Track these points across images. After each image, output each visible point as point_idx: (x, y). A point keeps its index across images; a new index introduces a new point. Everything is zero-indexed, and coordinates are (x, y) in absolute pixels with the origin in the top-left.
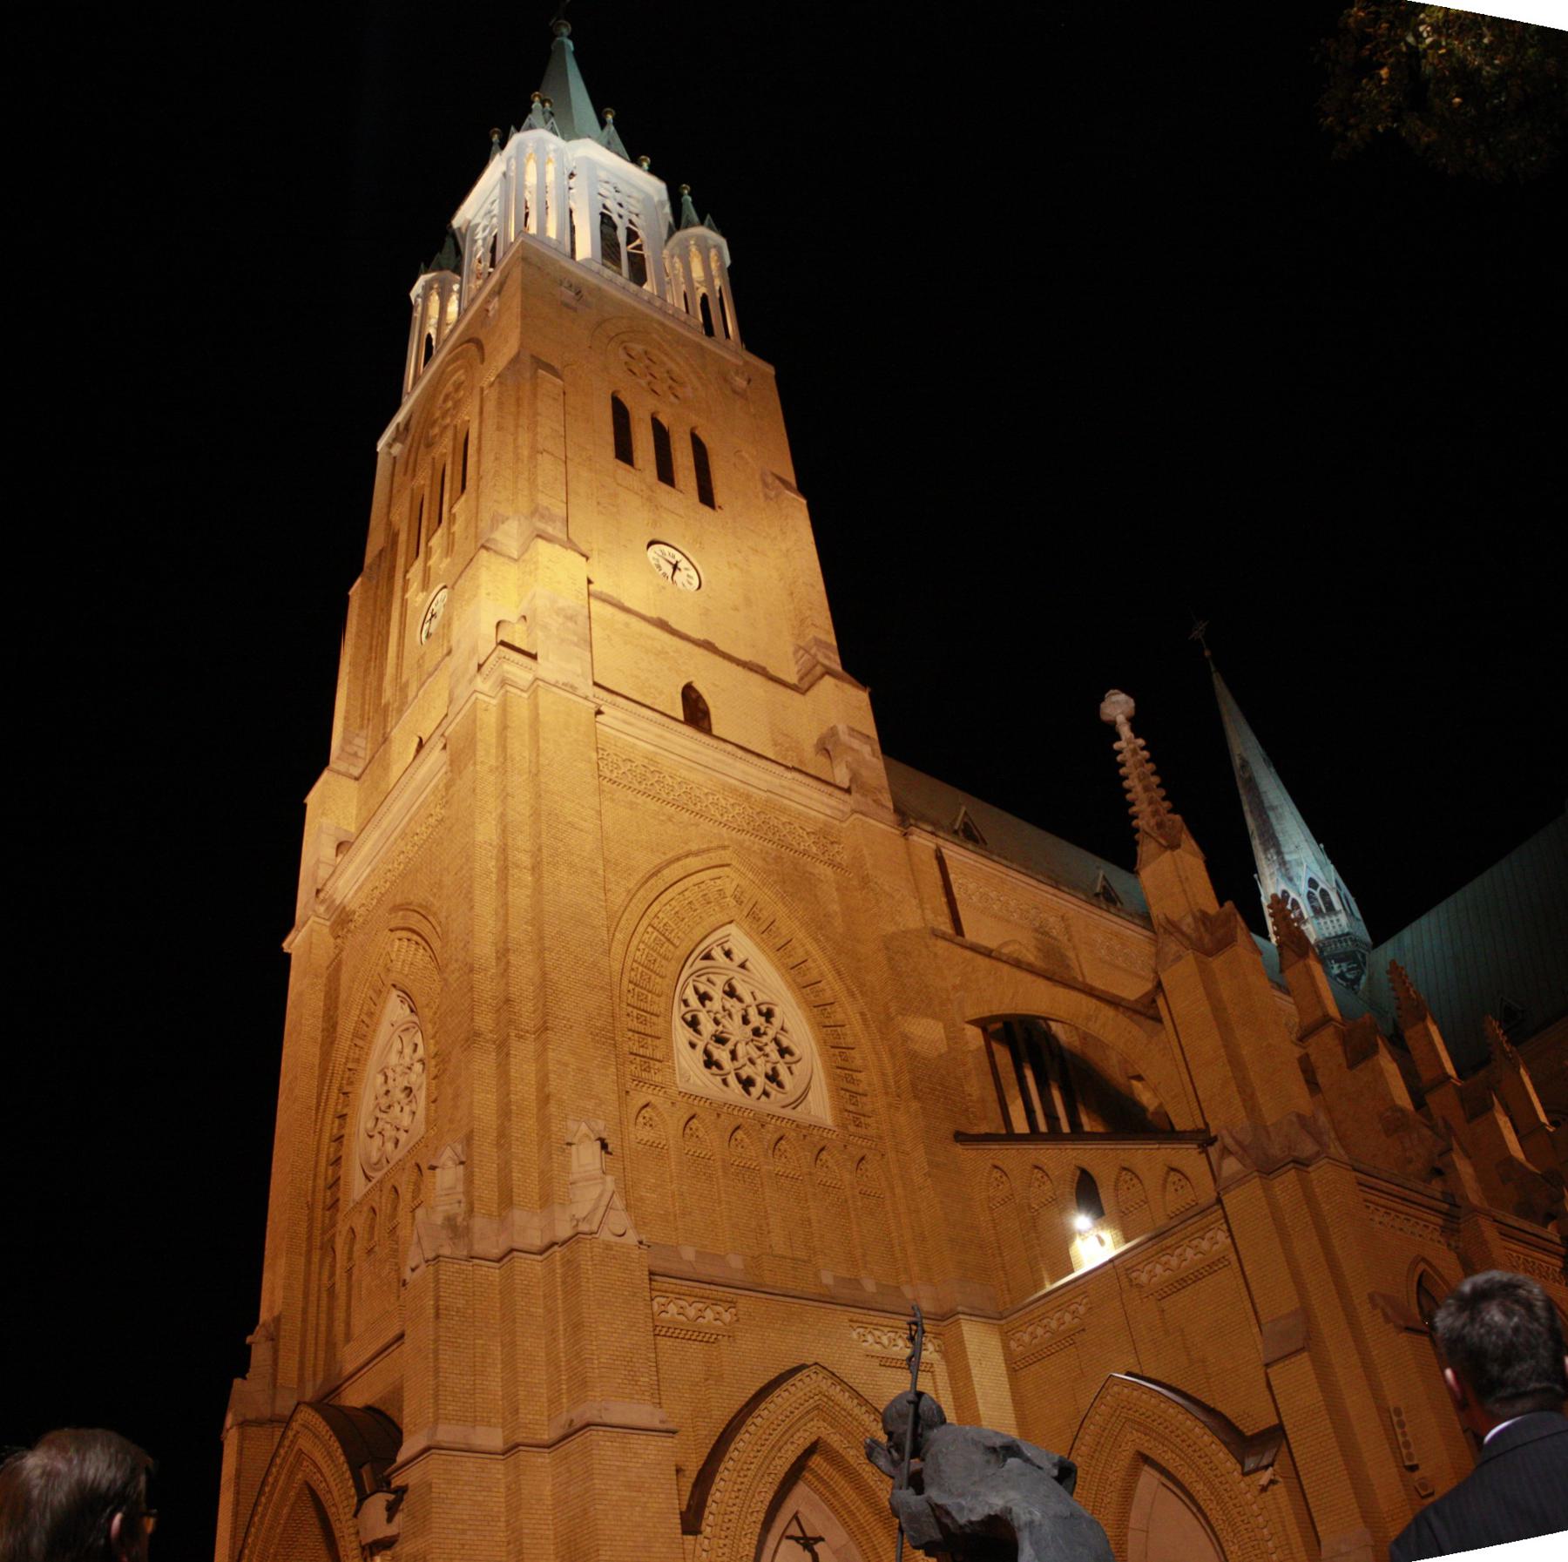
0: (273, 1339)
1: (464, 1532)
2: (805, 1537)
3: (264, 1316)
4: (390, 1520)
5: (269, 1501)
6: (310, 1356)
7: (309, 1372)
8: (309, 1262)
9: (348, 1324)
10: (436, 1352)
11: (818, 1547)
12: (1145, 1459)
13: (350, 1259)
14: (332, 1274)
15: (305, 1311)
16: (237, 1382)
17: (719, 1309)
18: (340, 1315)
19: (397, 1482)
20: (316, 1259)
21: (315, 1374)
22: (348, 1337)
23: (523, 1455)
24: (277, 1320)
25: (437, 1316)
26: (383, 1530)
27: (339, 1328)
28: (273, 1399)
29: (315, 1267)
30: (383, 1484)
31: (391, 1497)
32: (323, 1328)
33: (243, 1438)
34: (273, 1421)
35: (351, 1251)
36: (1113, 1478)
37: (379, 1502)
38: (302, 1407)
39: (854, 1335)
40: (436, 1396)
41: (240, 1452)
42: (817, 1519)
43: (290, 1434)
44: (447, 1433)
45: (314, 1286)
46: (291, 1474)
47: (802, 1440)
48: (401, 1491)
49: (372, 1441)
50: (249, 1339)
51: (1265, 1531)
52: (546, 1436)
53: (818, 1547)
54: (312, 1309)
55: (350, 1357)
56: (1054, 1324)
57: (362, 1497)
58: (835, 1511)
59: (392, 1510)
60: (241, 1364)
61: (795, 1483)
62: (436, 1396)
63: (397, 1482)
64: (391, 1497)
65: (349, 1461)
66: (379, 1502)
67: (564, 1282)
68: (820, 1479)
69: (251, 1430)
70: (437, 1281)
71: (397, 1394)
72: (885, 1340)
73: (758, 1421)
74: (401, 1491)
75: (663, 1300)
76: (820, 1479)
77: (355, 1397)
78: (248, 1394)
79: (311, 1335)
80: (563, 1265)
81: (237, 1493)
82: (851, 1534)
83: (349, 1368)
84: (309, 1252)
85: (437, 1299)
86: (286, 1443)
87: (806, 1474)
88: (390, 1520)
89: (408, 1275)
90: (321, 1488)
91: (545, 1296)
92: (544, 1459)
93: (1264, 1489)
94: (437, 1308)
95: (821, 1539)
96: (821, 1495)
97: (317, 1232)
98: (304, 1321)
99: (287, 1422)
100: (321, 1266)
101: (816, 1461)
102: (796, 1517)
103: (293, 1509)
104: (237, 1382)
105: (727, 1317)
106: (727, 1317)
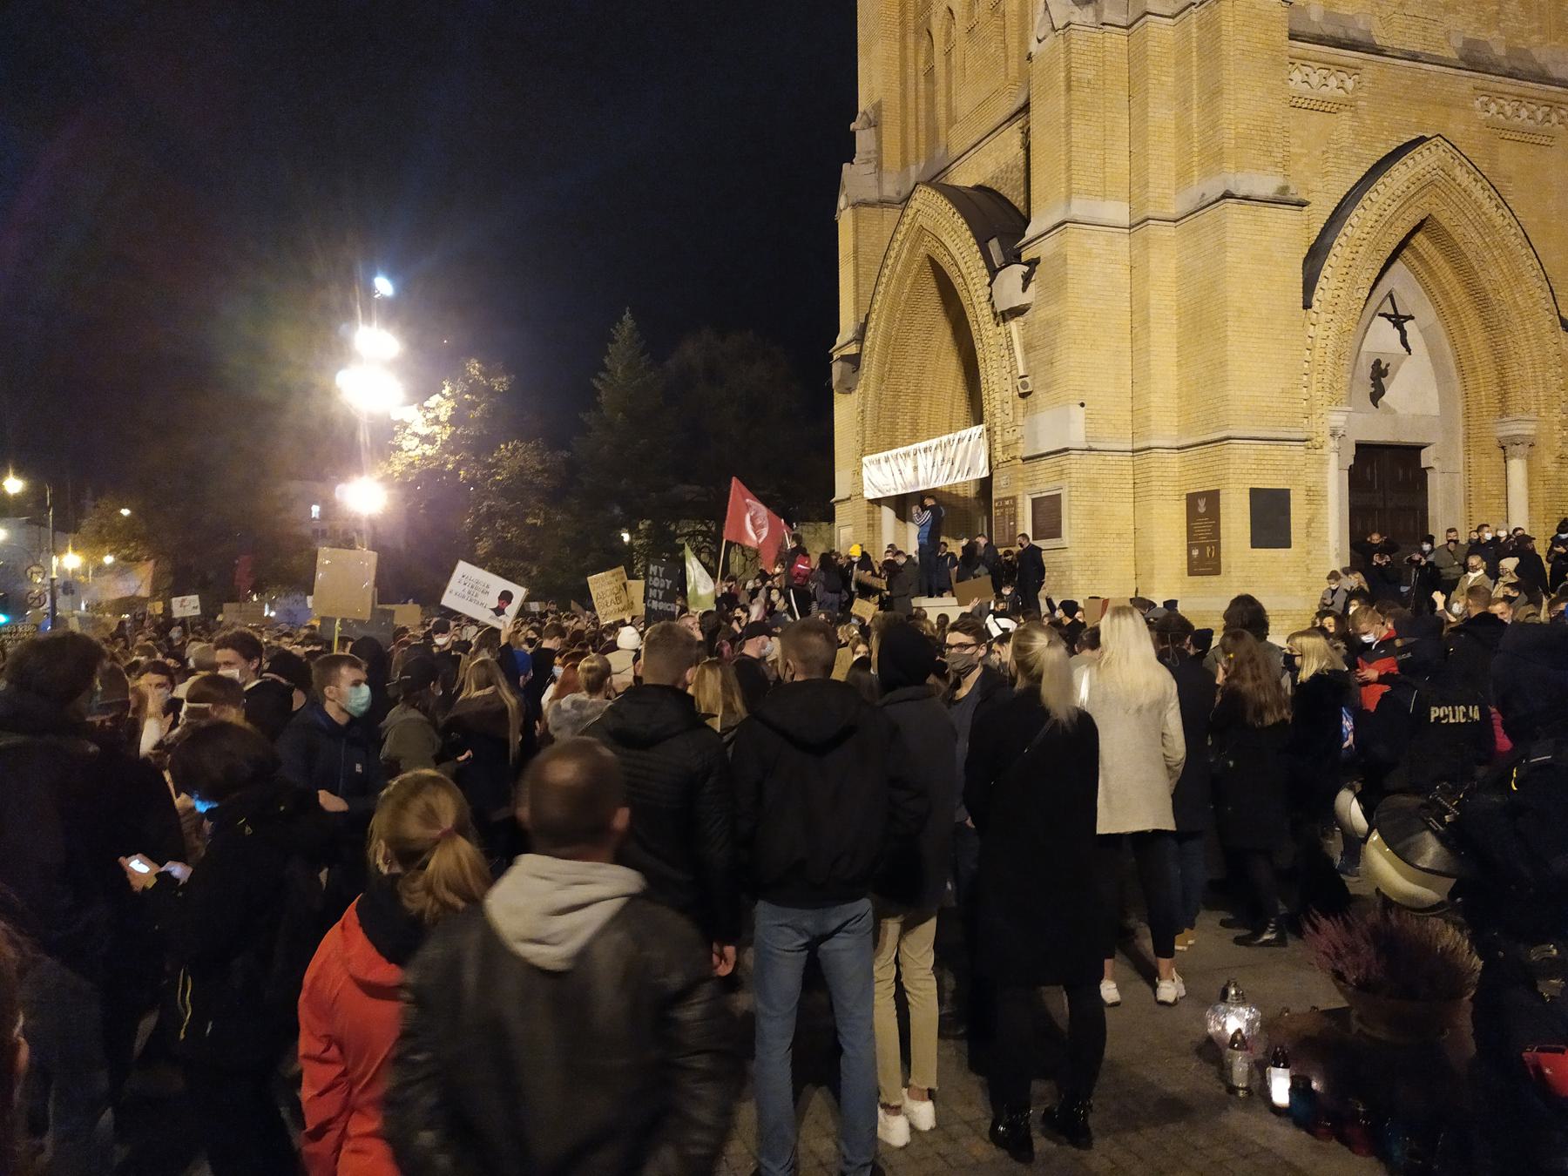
0: (875, 124)
2: (1396, 315)
3: (863, 104)
4: (1024, 290)
5: (893, 271)
7: (911, 157)
8: (904, 48)
9: (949, 105)
10: (1068, 125)
11: (1407, 325)
13: (947, 41)
15: (904, 96)
16: (846, 166)
18: (941, 99)
19: (1025, 256)
20: (911, 40)
21: (917, 157)
22: (951, 121)
24: (878, 107)
25: (1069, 88)
26: (1019, 299)
27: (941, 112)
28: (880, 181)
29: (910, 53)
30: (1013, 257)
31: (1026, 269)
32: (922, 114)
34: (883, 203)
35: (948, 33)
40: (1069, 168)
42: (1411, 298)
46: (911, 251)
47: (1413, 218)
48: (1033, 263)
50: (852, 126)
52: (1173, 211)
53: (1407, 325)
54: (911, 95)
55: (958, 140)
57: (993, 272)
60: (847, 151)
62: (1069, 168)
65: (975, 235)
66: (1018, 270)
67: (1199, 47)
69: (864, 210)
70: (1068, 51)
72: (1508, 110)
73: (1374, 196)
74: (1033, 263)
78: (856, 179)
79: (911, 120)
80: (1200, 28)
81: (857, 266)
82: (1440, 313)
83: (956, 150)
84: (903, 37)
85: (1069, 70)
88: (1024, 290)
89: (1034, 47)
90: (945, 262)
91: (1177, 64)
92: (1169, 231)
94: (1068, 80)
95: (1412, 318)
96: (1416, 274)
97: (910, 16)
100: (917, 52)
102: (1391, 296)
103: (915, 282)
104: (846, 166)
105: (1349, 84)
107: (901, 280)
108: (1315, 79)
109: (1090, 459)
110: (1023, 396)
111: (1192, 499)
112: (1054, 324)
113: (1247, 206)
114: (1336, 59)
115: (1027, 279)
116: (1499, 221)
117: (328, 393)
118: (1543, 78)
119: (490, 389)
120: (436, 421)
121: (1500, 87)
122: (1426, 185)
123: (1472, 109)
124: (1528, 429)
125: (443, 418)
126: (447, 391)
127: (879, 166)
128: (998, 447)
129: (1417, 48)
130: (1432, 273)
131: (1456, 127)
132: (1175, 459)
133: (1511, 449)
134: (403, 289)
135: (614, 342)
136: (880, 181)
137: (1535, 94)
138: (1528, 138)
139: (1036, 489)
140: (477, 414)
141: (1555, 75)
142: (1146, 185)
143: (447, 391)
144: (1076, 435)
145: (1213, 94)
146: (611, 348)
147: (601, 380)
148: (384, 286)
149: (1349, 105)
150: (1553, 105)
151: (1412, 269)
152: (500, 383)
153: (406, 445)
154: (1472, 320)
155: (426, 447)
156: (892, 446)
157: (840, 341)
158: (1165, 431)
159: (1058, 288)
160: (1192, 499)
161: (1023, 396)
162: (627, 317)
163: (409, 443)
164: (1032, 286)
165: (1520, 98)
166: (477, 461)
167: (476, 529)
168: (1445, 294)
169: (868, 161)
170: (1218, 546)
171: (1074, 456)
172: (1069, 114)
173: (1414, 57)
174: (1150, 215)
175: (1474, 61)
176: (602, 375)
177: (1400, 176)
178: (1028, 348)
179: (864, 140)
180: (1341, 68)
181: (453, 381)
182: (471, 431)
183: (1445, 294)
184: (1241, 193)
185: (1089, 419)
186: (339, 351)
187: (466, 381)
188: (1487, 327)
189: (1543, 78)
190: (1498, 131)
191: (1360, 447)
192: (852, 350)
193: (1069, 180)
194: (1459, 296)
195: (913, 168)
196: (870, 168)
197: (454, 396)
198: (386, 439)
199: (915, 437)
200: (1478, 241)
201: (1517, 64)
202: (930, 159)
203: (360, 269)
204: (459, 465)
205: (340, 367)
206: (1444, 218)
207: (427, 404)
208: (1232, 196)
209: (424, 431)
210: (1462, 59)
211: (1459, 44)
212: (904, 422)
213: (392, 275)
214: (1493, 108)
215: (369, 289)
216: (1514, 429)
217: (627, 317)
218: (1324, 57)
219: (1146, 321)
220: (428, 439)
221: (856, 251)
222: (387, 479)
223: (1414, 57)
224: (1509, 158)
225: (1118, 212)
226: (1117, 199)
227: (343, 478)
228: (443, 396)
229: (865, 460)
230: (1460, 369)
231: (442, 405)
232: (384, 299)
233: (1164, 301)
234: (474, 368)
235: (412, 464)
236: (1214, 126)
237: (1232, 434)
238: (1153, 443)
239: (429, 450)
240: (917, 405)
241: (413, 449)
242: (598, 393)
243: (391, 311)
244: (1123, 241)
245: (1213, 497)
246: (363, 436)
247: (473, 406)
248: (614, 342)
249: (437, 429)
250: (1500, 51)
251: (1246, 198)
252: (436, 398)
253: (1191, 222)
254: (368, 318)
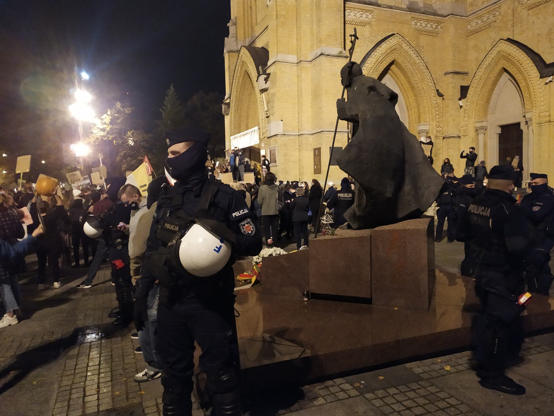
0: (235, 24)
1: (286, 87)
3: (232, 17)
4: (266, 83)
6: (247, 30)
9: (256, 19)
10: (277, 30)
12: (506, 70)
14: (251, 3)
15: (244, 15)
16: (226, 38)
17: (367, 13)
18: (254, 16)
19: (268, 72)
22: (257, 24)
23: (303, 64)
24: (236, 18)
25: (277, 18)
26: (264, 86)
27: (254, 21)
31: (266, 76)
32: (250, 21)
33: (229, 56)
36: (491, 76)
37: (263, 77)
38: (243, 47)
39: (413, 23)
41: (229, 60)
43: (240, 55)
44: (280, 57)
45: (246, 6)
46: (241, 68)
47: (389, 61)
48: (269, 75)
49: (261, 57)
50: (228, 25)
51: (542, 99)
52: (310, 59)
54: (246, 14)
55: (258, 31)
56: (485, 19)
57: (259, 75)
58: (397, 83)
59: (266, 80)
61: (386, 74)
63: (268, 72)
64: (266, 76)
66: (263, 77)
67: (316, 5)
68: (393, 73)
69: (231, 54)
71: (267, 44)
75: (349, 11)
76: (393, 73)
77: (259, 44)
78: (229, 43)
79: (246, 23)
83: (257, 35)
85: (277, 11)
86: (240, 58)
87: (390, 71)
88: (266, 83)
92: (308, 65)
93: (546, 84)
96: (393, 78)
98: (244, 18)
99: (239, 51)
101: (393, 67)
103: (243, 79)
104: (226, 38)
105: (370, 17)
106: (370, 17)
107: (239, 79)
108: (358, 15)
109: (285, 138)
110: (267, 117)
111: (315, 150)
112: (274, 94)
113: (328, 58)
114: (364, 8)
115: (266, 80)
116: (418, 61)
117: (64, 112)
118: (435, 14)
119: (124, 112)
120: (105, 123)
121: (421, 17)
122: (393, 50)
123: (412, 24)
124: (426, 128)
125: (108, 122)
126: (109, 113)
127: (236, 38)
128: (261, 134)
129: (392, 4)
130: (398, 78)
131: (405, 30)
132: (311, 137)
133: (479, 131)
134: (92, 76)
135: (168, 96)
136: (237, 43)
137: (432, 19)
138: (432, 34)
139: (272, 146)
140: (119, 121)
141: (440, 13)
142: (301, 50)
143: (109, 113)
144: (280, 131)
145: (319, 21)
146: (166, 98)
147: (163, 109)
148: (85, 76)
149: (369, 23)
150: (439, 23)
151: (392, 76)
152: (128, 111)
153: (94, 131)
154: (411, 94)
155: (102, 132)
156: (239, 132)
157: (226, 98)
158: (308, 128)
159: (274, 83)
160: (315, 150)
161: (267, 117)
162: (172, 87)
163: (95, 131)
164: (268, 82)
165: (428, 20)
166: (120, 137)
167: (121, 161)
168: (402, 85)
169: (233, 37)
170: (320, 164)
171: (279, 137)
172: (277, 26)
173: (391, 7)
174: (302, 60)
175: (412, 9)
176: (163, 107)
177: (384, 46)
178: (268, 102)
179: (232, 30)
180: (367, 11)
181: (111, 109)
182: (117, 127)
183: (402, 85)
184: (326, 53)
185: (284, 125)
186: (69, 97)
187: (116, 109)
188: (415, 96)
189: (435, 14)
190: (420, 32)
191: (503, 127)
192: (228, 101)
193: (277, 48)
194: (406, 85)
195: (247, 40)
196: (234, 39)
197: (111, 115)
198: (88, 131)
199: (247, 129)
200: (411, 67)
201: (426, 9)
202: (252, 37)
203: (76, 68)
204: (113, 139)
205: (70, 104)
206: (399, 60)
207: (102, 117)
208: (323, 55)
209: (102, 127)
210: (408, 8)
211: (407, 3)
212: (243, 125)
213: (88, 72)
214: (419, 24)
215: (80, 77)
216: (422, 128)
217: (172, 87)
218: (361, 8)
219: (301, 94)
220: (103, 130)
221: (229, 68)
222: (89, 143)
223: (391, 7)
224: (424, 40)
225: (293, 58)
226: (293, 54)
227: (72, 142)
228: (108, 115)
229: (231, 137)
230: (407, 109)
231: (107, 118)
232: (85, 81)
233: (307, 87)
234: (118, 105)
235: (97, 139)
236: (319, 31)
237: (323, 130)
238: (303, 133)
239: (102, 133)
240: (247, 119)
241: (98, 133)
242: (161, 113)
243: (89, 85)
244: (295, 68)
245: (319, 149)
246: (81, 130)
247: (118, 118)
248: (168, 96)
249: (105, 126)
250: (421, 5)
251: (328, 55)
252: (105, 115)
253: (314, 62)
254: (80, 87)
